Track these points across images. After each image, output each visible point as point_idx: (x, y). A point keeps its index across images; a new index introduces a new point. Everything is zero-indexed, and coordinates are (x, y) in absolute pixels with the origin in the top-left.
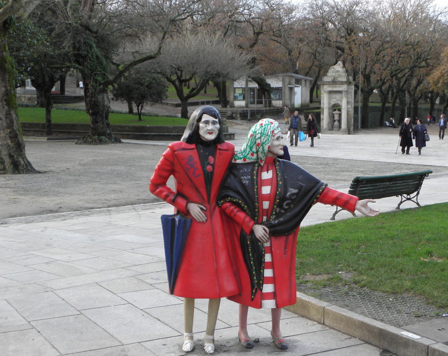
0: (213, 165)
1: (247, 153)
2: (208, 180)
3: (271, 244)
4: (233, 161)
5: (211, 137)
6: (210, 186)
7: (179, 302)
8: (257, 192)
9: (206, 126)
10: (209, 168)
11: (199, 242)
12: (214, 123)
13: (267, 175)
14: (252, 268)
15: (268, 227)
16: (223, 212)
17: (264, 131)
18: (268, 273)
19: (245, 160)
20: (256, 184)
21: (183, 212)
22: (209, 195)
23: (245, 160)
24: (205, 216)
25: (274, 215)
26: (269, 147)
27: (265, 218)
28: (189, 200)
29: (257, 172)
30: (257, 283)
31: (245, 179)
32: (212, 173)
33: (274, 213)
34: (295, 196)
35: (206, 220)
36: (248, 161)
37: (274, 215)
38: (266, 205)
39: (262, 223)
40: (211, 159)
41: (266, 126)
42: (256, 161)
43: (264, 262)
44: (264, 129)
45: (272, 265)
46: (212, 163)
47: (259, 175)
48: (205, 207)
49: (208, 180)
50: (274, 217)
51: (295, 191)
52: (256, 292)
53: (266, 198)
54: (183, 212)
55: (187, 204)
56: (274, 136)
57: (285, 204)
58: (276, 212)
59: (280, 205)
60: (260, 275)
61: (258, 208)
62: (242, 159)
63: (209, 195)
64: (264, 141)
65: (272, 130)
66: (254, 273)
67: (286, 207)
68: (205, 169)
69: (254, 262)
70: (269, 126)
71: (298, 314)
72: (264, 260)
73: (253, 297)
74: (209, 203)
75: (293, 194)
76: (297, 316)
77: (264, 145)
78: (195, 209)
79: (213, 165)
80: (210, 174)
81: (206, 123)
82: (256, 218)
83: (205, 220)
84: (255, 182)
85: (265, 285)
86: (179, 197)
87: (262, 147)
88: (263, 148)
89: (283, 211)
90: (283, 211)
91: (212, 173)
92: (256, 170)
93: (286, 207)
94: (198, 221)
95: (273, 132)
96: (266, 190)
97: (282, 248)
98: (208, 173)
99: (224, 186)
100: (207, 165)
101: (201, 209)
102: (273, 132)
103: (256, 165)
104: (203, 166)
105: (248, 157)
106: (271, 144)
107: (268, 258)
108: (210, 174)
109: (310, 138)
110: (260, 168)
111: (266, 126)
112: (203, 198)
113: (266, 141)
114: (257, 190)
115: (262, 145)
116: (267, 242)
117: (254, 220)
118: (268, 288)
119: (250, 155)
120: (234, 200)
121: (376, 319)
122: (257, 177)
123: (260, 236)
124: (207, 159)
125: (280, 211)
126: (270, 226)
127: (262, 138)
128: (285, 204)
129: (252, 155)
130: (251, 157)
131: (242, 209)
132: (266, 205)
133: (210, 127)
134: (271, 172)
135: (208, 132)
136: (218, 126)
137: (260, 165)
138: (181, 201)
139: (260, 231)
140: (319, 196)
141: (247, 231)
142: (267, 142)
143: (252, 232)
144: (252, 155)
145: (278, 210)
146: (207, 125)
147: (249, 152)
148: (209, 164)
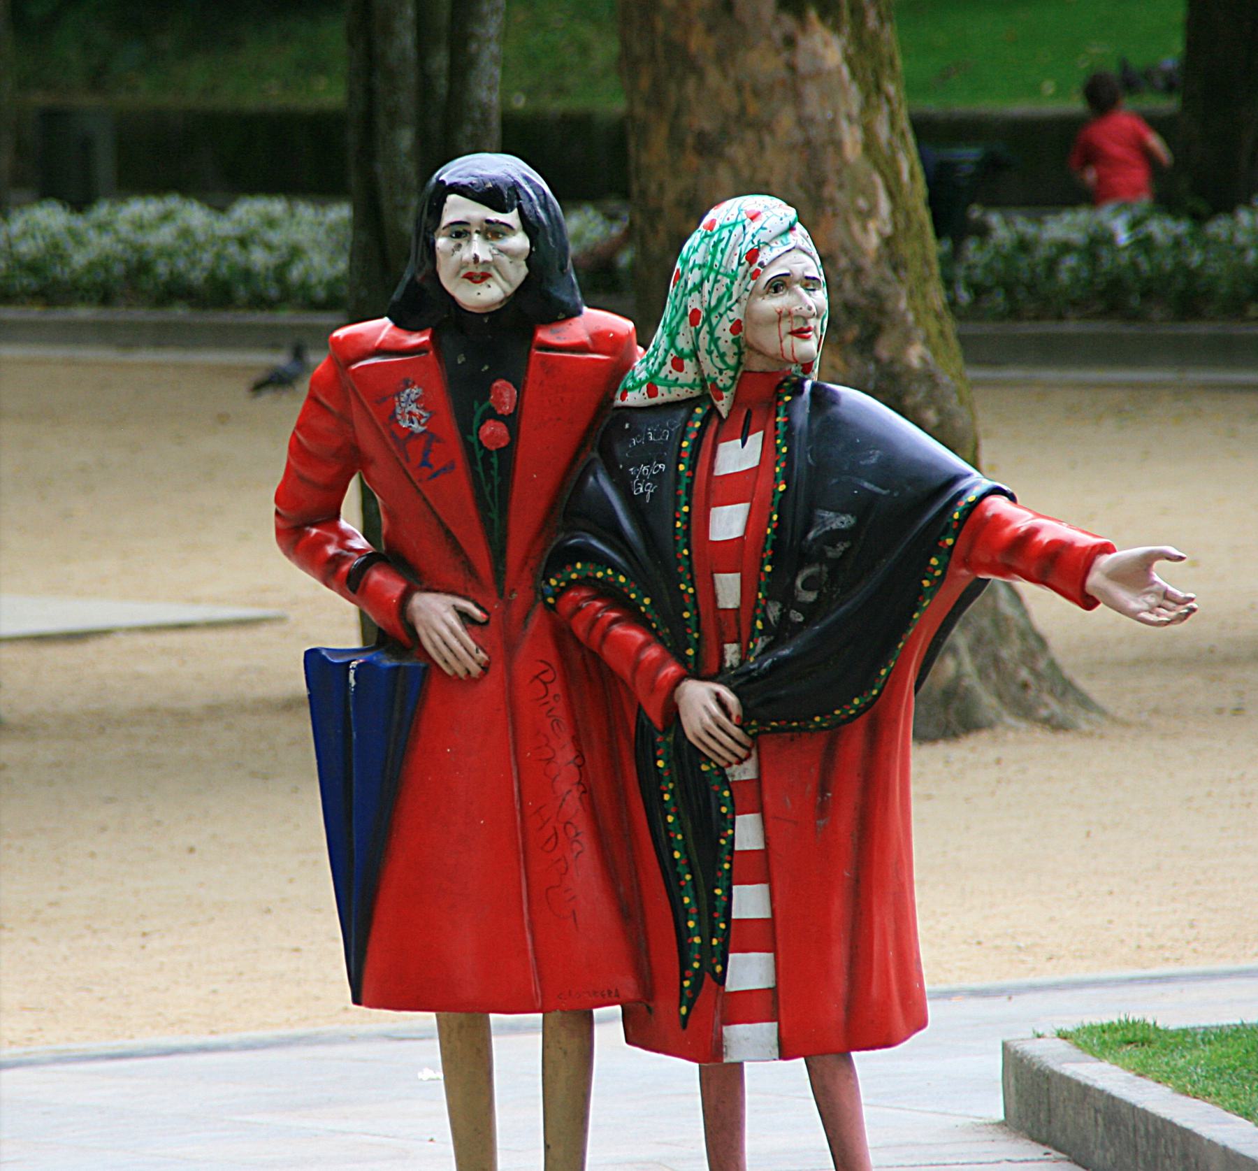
0: (512, 421)
1: (660, 359)
2: (487, 489)
3: (760, 768)
4: (618, 402)
5: (491, 293)
6: (504, 511)
7: (412, 1042)
8: (687, 533)
9: (459, 246)
10: (493, 432)
11: (462, 766)
12: (492, 231)
13: (737, 457)
14: (679, 877)
15: (734, 691)
16: (562, 634)
17: (714, 257)
18: (750, 902)
19: (652, 391)
20: (684, 499)
21: (393, 635)
22: (499, 554)
23: (652, 391)
24: (473, 646)
25: (762, 633)
26: (737, 327)
27: (732, 653)
28: (418, 580)
29: (697, 444)
30: (701, 946)
31: (641, 477)
32: (507, 454)
33: (759, 625)
34: (841, 547)
35: (485, 668)
36: (664, 395)
37: (762, 633)
38: (729, 590)
39: (716, 674)
40: (505, 395)
41: (725, 233)
42: (697, 392)
43: (732, 851)
44: (715, 245)
45: (759, 868)
46: (507, 409)
47: (703, 451)
48: (478, 606)
49: (487, 489)
50: (761, 644)
51: (844, 521)
52: (696, 988)
53: (730, 555)
54: (393, 635)
55: (406, 597)
56: (756, 275)
57: (799, 583)
58: (765, 621)
59: (781, 590)
60: (716, 910)
61: (696, 604)
62: (644, 388)
63: (499, 554)
64: (713, 303)
65: (747, 246)
66: (687, 900)
67: (811, 597)
68: (473, 439)
69: (685, 852)
70: (739, 228)
71: (1069, 1154)
72: (732, 841)
73: (684, 1010)
74: (501, 594)
75: (834, 537)
76: (1060, 1155)
77: (714, 321)
78: (438, 616)
79: (512, 421)
80: (495, 460)
81: (458, 235)
82: (690, 652)
83: (475, 669)
84: (682, 488)
85: (735, 959)
86: (379, 574)
87: (706, 328)
88: (711, 332)
89: (797, 617)
90: (797, 617)
91: (507, 454)
92: (692, 436)
93: (811, 597)
94: (448, 671)
95: (753, 255)
96: (728, 522)
97: (809, 788)
98: (488, 453)
99: (572, 507)
100: (482, 422)
101: (463, 615)
102: (753, 255)
103: (698, 410)
104: (466, 428)
105: (662, 375)
106: (748, 313)
107: (747, 833)
108: (495, 460)
109: (587, 339)
110: (715, 422)
111: (725, 233)
112: (470, 569)
113: (720, 300)
114: (687, 523)
115: (707, 319)
116: (740, 761)
117: (682, 660)
118: (749, 971)
119: (669, 366)
120: (600, 574)
121: (1187, 1094)
122: (692, 468)
123: (698, 728)
124: (484, 390)
125: (784, 616)
126: (741, 682)
127: (707, 286)
128: (799, 583)
129: (678, 365)
130: (676, 374)
131: (633, 616)
132: (729, 590)
133: (478, 248)
134: (756, 440)
135: (463, 272)
136: (519, 241)
137: (713, 410)
138: (386, 582)
139: (701, 702)
140: (950, 541)
141: (654, 713)
142: (726, 303)
143: (672, 714)
144: (678, 365)
145: (774, 611)
146: (463, 242)
147: (666, 351)
148: (491, 414)
